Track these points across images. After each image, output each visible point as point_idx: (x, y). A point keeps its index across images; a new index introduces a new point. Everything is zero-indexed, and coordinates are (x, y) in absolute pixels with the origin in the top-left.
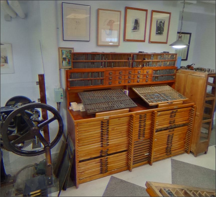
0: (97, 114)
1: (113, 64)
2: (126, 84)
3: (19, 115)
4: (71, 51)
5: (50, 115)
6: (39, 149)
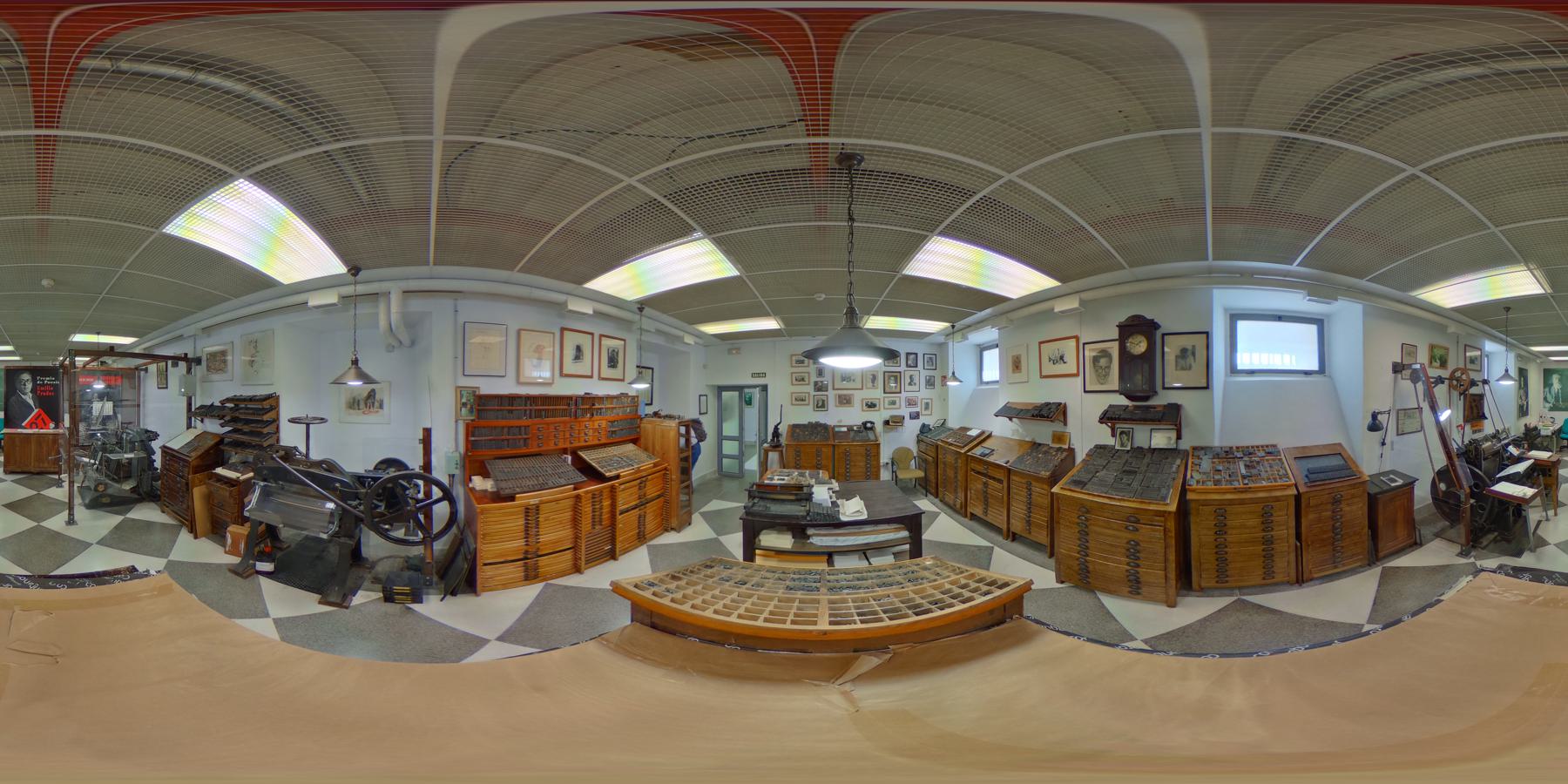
0: (517, 496)
1: (544, 413)
2: (567, 445)
3: (390, 485)
4: (475, 392)
5: (437, 493)
6: (415, 538)
